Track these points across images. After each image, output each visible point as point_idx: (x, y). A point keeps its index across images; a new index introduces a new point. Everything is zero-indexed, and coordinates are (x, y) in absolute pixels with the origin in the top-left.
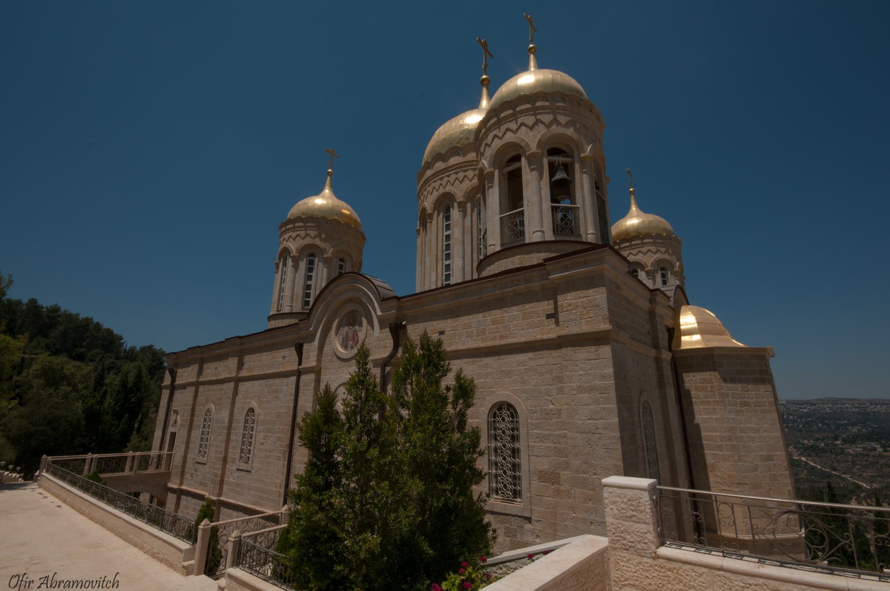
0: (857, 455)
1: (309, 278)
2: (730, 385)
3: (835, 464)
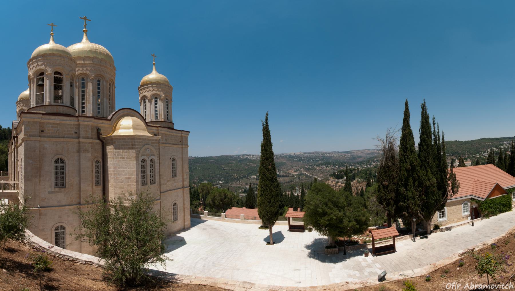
0: (319, 170)
1: (156, 107)
2: (117, 150)
3: (313, 173)
